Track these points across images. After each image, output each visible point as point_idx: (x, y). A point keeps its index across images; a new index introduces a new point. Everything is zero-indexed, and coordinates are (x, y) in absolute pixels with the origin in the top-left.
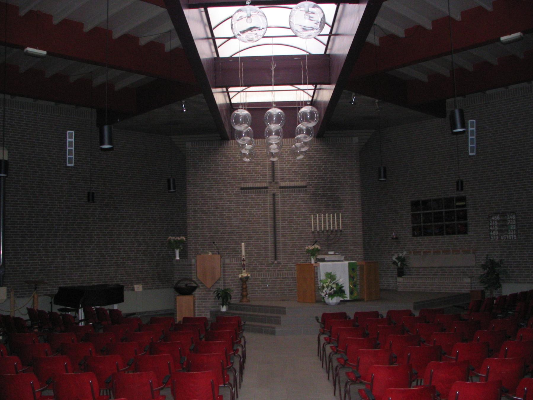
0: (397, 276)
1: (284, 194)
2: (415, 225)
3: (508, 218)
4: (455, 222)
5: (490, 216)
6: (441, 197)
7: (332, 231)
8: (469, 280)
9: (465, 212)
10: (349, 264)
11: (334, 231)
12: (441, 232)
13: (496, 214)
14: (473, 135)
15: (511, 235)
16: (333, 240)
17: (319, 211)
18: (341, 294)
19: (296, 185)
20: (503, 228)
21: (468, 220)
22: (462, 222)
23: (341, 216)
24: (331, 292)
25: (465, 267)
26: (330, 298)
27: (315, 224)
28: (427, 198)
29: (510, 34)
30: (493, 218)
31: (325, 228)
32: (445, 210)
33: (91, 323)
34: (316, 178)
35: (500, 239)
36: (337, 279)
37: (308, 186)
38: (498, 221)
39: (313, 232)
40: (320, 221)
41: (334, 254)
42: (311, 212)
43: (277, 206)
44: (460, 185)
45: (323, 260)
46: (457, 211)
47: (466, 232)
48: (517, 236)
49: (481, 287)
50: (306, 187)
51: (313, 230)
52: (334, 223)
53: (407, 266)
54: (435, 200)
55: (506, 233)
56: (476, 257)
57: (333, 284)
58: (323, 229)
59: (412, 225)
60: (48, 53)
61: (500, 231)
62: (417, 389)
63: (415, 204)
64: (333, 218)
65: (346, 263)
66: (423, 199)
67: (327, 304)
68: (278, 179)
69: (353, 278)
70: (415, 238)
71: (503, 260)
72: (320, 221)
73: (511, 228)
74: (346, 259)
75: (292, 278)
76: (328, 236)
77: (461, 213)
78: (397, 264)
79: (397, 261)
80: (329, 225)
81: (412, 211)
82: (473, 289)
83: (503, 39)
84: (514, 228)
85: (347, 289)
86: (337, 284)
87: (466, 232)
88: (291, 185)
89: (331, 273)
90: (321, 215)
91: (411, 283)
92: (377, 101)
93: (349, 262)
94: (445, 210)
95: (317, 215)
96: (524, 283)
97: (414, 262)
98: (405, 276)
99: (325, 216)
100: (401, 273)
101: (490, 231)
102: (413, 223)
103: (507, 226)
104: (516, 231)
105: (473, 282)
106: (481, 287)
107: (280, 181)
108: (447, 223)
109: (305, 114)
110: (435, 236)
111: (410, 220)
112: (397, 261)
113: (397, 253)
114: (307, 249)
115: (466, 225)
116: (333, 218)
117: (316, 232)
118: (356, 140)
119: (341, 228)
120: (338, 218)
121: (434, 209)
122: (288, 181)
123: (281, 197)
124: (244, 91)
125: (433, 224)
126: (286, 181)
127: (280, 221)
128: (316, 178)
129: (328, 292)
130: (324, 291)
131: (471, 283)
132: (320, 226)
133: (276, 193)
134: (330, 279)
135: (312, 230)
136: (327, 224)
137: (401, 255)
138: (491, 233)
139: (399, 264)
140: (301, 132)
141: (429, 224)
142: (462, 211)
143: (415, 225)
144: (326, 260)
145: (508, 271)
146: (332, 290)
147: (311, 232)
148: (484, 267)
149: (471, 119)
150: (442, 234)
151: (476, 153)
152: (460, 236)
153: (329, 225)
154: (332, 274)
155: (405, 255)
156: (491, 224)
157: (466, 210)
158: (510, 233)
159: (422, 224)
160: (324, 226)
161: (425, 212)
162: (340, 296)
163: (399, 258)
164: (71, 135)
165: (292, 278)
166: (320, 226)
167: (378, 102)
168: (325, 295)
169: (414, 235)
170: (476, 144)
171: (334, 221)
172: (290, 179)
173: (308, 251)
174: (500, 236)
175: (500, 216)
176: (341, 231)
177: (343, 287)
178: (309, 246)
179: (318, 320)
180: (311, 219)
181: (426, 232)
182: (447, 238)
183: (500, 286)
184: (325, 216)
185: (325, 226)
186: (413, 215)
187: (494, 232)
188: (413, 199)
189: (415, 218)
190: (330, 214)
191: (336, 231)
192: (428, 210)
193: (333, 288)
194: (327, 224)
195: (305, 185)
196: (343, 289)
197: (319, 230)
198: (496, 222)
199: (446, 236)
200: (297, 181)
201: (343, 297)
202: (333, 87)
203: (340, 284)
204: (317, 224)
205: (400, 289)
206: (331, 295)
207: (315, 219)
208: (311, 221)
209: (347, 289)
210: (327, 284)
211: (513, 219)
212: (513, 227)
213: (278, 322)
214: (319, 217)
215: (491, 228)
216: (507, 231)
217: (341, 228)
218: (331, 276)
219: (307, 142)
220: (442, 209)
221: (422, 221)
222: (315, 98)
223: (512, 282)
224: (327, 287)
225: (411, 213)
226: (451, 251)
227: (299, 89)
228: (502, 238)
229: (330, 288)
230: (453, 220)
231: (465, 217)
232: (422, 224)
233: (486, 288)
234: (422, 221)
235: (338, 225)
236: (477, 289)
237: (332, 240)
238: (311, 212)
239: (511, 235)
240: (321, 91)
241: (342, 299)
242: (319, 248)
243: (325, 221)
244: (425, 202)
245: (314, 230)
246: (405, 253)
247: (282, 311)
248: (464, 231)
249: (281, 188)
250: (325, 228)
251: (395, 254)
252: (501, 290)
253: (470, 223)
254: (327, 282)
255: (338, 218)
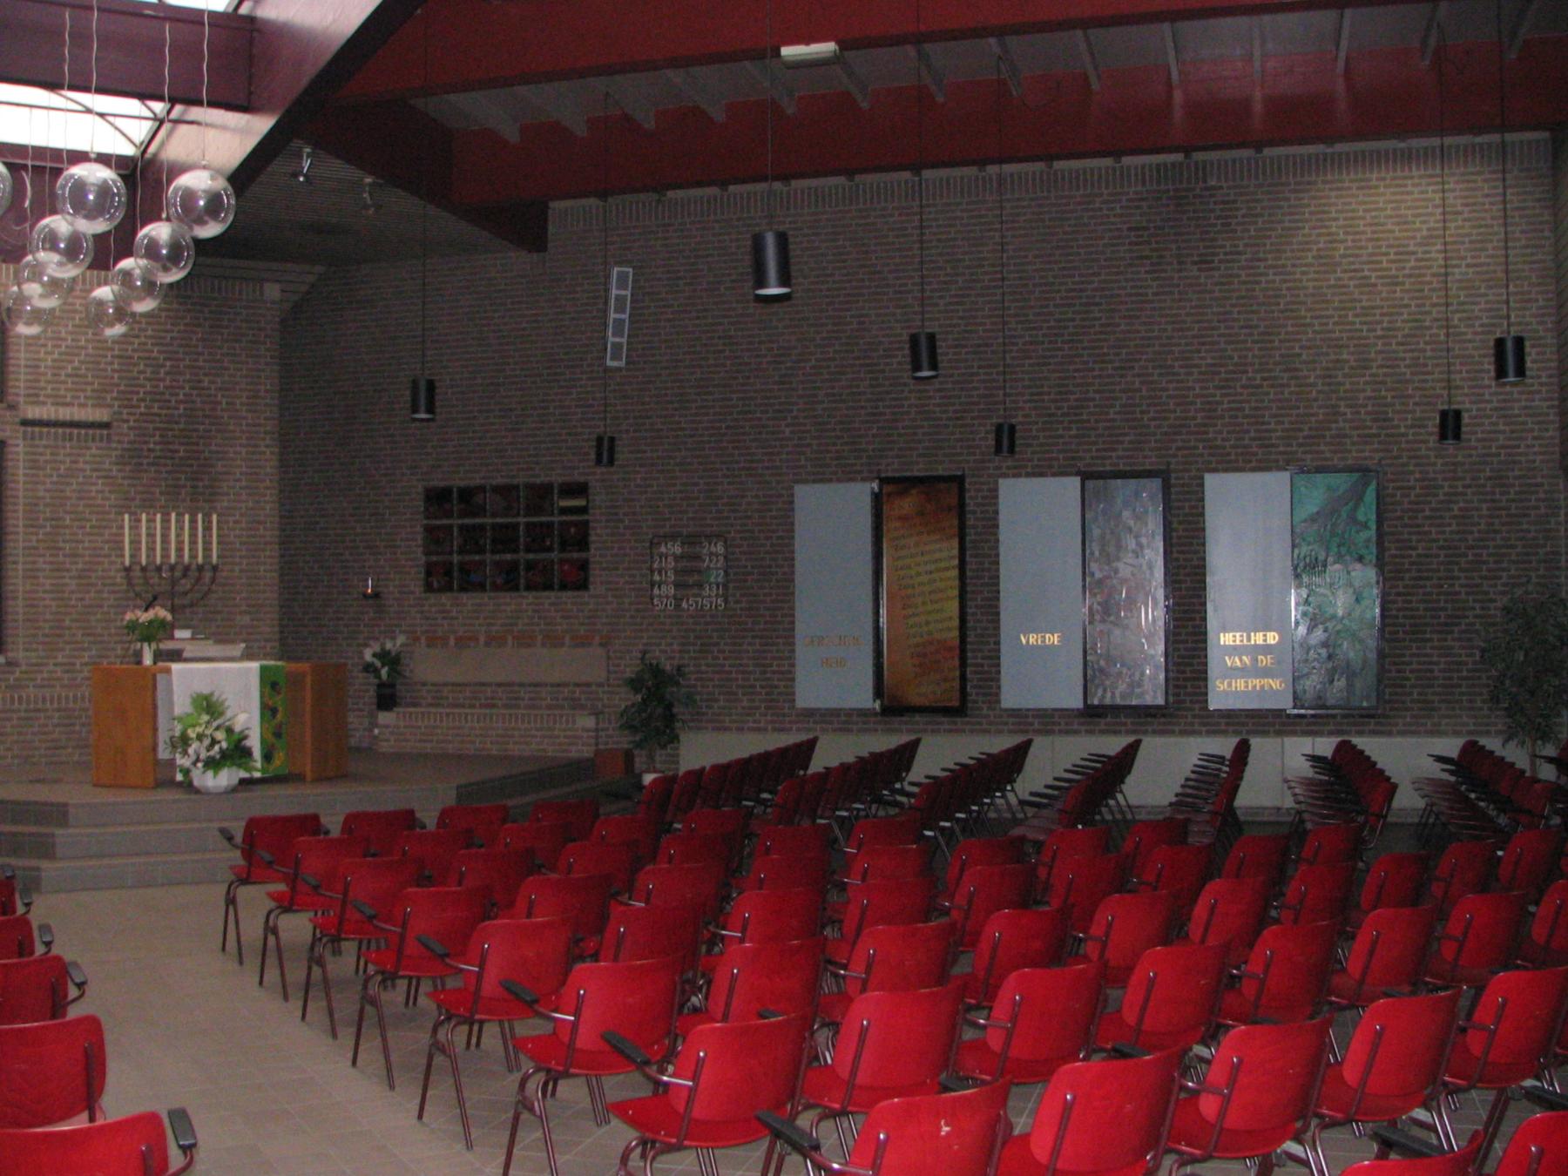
0: (374, 707)
1: (37, 442)
2: (434, 558)
3: (705, 551)
4: (555, 555)
5: (655, 541)
6: (515, 481)
7: (187, 569)
8: (589, 722)
9: (584, 528)
10: (263, 670)
11: (194, 567)
12: (510, 581)
13: (673, 537)
14: (623, 311)
15: (711, 598)
16: (189, 596)
17: (149, 504)
18: (243, 760)
19: (76, 418)
20: (689, 576)
21: (592, 551)
22: (575, 555)
23: (218, 522)
24: (212, 753)
25: (577, 685)
26: (210, 773)
27: (135, 543)
28: (472, 483)
29: (807, 44)
30: (663, 549)
31: (165, 555)
32: (460, 522)
33: (929, 837)
34: (143, 400)
35: (678, 606)
36: (229, 714)
37: (115, 424)
38: (677, 558)
39: (128, 570)
40: (151, 535)
41: (193, 639)
42: (122, 507)
43: (13, 482)
44: (605, 451)
45: (177, 656)
46: (561, 523)
47: (583, 585)
48: (726, 602)
49: (624, 741)
50: (107, 425)
51: (127, 563)
52: (193, 542)
53: (405, 677)
54: (497, 490)
55: (696, 591)
56: (609, 658)
57: (217, 728)
58: (158, 561)
59: (424, 558)
60: (844, 45)
61: (677, 585)
62: (779, 1022)
63: (437, 498)
64: (193, 528)
65: (255, 666)
66: (462, 484)
67: (197, 791)
68: (17, 395)
69: (274, 711)
70: (432, 595)
71: (684, 666)
72: (151, 535)
73: (712, 580)
74: (248, 656)
75: (59, 710)
76: (174, 582)
77: (573, 530)
78: (376, 671)
79: (378, 663)
80: (180, 550)
81: (427, 518)
82: (601, 747)
83: (787, 51)
84: (720, 580)
85: (254, 743)
86: (230, 731)
87: (583, 585)
88: (61, 417)
89: (212, 694)
90: (155, 515)
91: (420, 727)
92: (368, 180)
93: (265, 662)
94: (525, 520)
95: (144, 516)
96: (740, 730)
97: (427, 667)
98: (401, 710)
99: (166, 521)
100: (387, 699)
101: (652, 584)
102: (427, 554)
103: (699, 572)
104: (725, 586)
105: (601, 726)
106: (624, 741)
107: (25, 402)
108: (531, 556)
109: (80, 187)
110: (492, 594)
111: (420, 542)
112: (378, 663)
113: (377, 639)
114: (131, 621)
115: (584, 566)
116: (193, 528)
117: (138, 568)
118: (272, 291)
119: (214, 560)
120: (207, 528)
121: (494, 515)
122: (53, 404)
123: (26, 453)
124: (80, 108)
125: (488, 557)
126: (44, 403)
127: (21, 529)
128: (143, 400)
129: (203, 755)
130: (191, 751)
131: (597, 730)
132: (151, 549)
133: (11, 438)
134: (208, 713)
135: (123, 563)
136: (173, 546)
137: (389, 646)
138: (656, 591)
139: (384, 672)
140: (51, 241)
141: (477, 558)
142: (575, 524)
143: (434, 558)
144: (185, 655)
145: (698, 698)
146: (217, 748)
147: (119, 566)
148: (635, 684)
149: (619, 264)
150: (516, 588)
151: (627, 363)
152: (567, 596)
153: (180, 550)
154: (214, 699)
155: (401, 646)
156: (655, 566)
157: (587, 523)
158: (707, 592)
159: (456, 558)
160: (163, 549)
161: (467, 521)
162: (239, 766)
163: (383, 655)
164: (622, 278)
165: (59, 710)
166: (151, 549)
167: (370, 185)
168: (194, 764)
169: (429, 588)
170: (629, 336)
171: (193, 535)
172: (56, 396)
173: (133, 626)
174: (678, 600)
175: (683, 543)
176: (215, 568)
177: (246, 737)
178: (139, 613)
179: (230, 839)
180: (122, 527)
181: (466, 579)
182: (528, 600)
183: (675, 739)
184: (166, 521)
185: (165, 550)
186: (429, 530)
187: (664, 588)
188: (435, 483)
189: (434, 537)
190: (183, 515)
191: (200, 568)
192: (475, 515)
193: (219, 742)
194: (173, 546)
195: (105, 419)
196: (247, 743)
197: (148, 564)
198: (670, 559)
199: (525, 594)
200: (80, 405)
201: (248, 769)
202: (259, 125)
203: (237, 728)
204: (140, 542)
205: (385, 747)
206: (213, 764)
207: (135, 526)
208: (123, 535)
209: (254, 743)
210: (199, 729)
211: (717, 555)
212: (717, 576)
213: (46, 849)
214: (148, 521)
215: (657, 578)
216: (700, 586)
217: (214, 560)
218: (209, 706)
219: (63, 280)
220: (518, 515)
221: (455, 548)
222: (152, 149)
223: (706, 728)
224: (200, 737)
225: (425, 522)
226: (540, 638)
227: (89, 111)
228: (684, 605)
229: (207, 742)
230: (550, 549)
231: (583, 543)
232: (456, 558)
233: (639, 745)
234: (455, 548)
235: (207, 549)
236: (610, 746)
237: (186, 593)
238: (122, 507)
239: (711, 598)
240: (183, 128)
241: (243, 774)
242: (169, 617)
243: (165, 538)
244: (466, 494)
245: (132, 563)
246: (401, 639)
247: (58, 814)
248: (578, 579)
249: (26, 423)
250: (165, 555)
251: (371, 642)
252: (677, 749)
253: (597, 558)
254: (200, 725)
255: (207, 528)
